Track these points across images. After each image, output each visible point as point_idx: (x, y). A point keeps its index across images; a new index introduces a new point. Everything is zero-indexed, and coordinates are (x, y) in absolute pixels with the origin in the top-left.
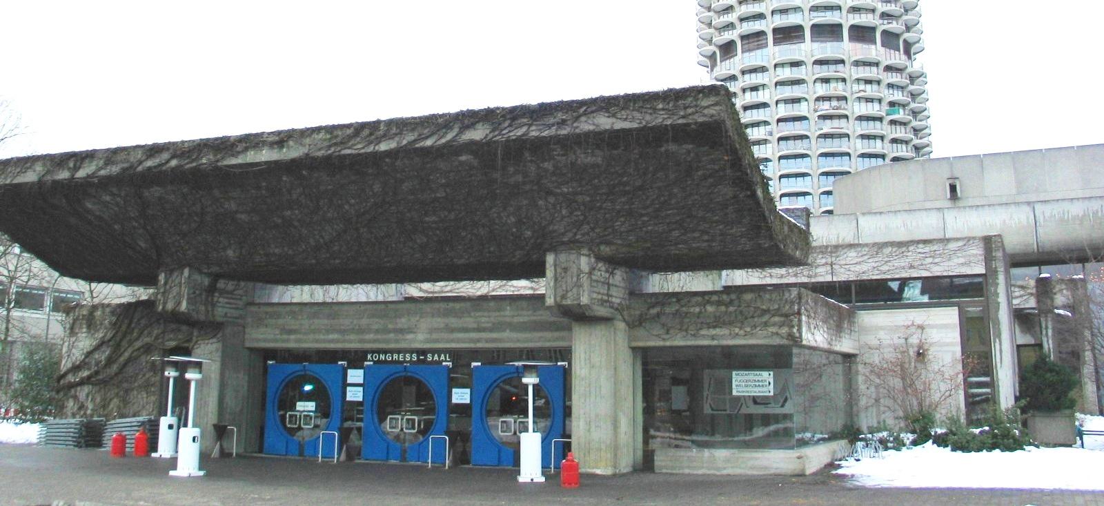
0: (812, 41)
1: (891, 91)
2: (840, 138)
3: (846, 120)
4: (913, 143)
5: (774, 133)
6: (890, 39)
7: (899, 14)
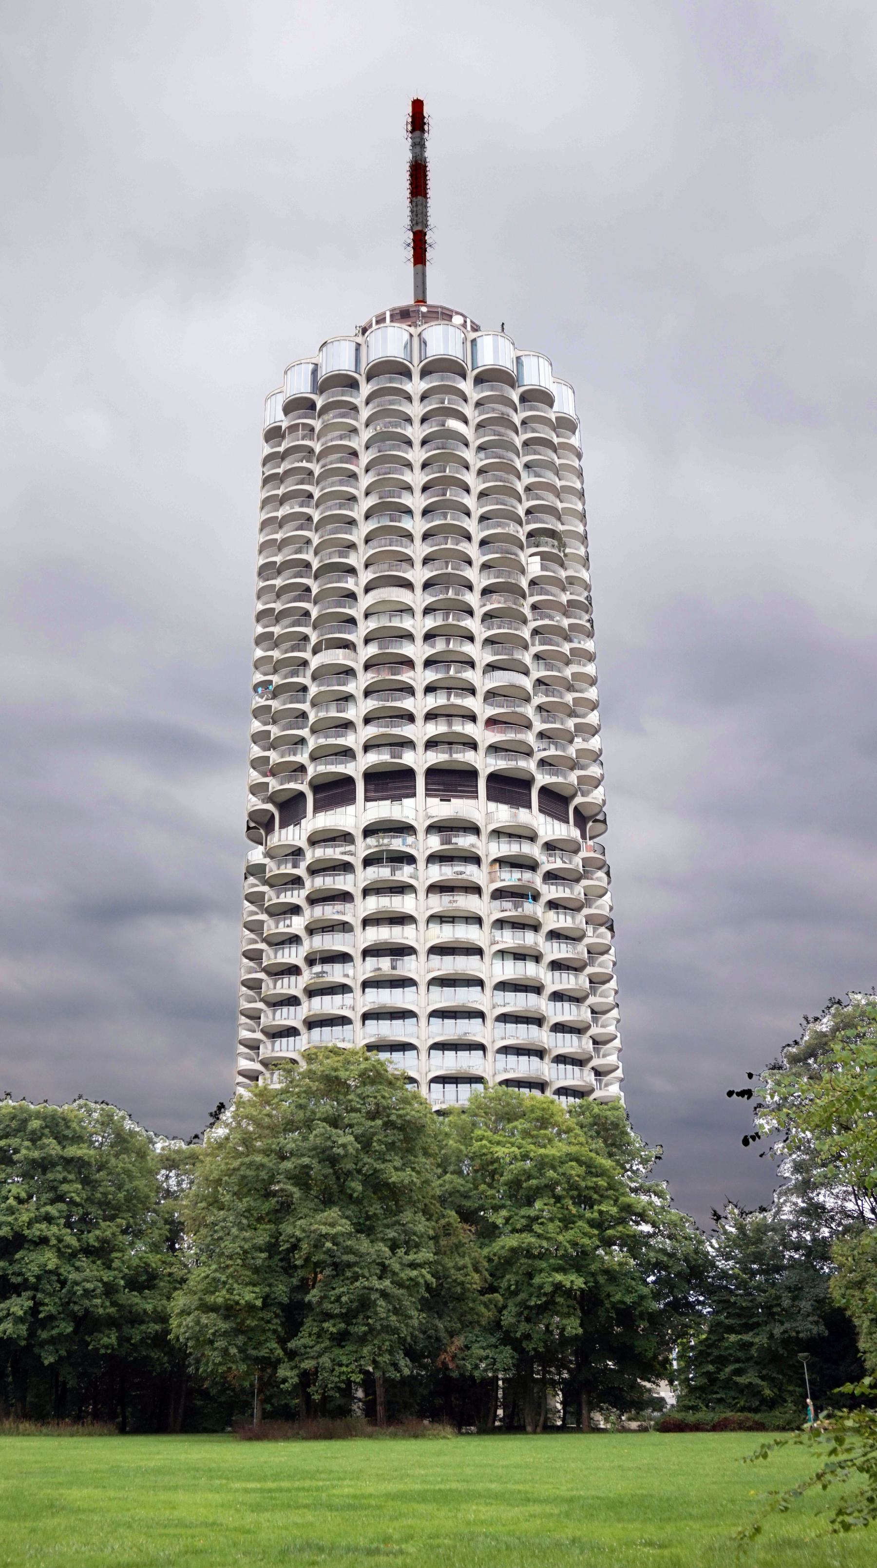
0: (427, 795)
1: (556, 945)
2: (470, 1050)
3: (481, 1052)
4: (591, 1032)
5: (357, 1008)
6: (555, 801)
7: (583, 994)
